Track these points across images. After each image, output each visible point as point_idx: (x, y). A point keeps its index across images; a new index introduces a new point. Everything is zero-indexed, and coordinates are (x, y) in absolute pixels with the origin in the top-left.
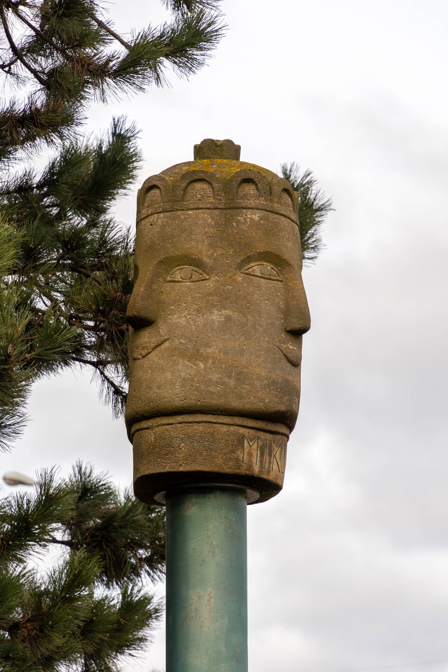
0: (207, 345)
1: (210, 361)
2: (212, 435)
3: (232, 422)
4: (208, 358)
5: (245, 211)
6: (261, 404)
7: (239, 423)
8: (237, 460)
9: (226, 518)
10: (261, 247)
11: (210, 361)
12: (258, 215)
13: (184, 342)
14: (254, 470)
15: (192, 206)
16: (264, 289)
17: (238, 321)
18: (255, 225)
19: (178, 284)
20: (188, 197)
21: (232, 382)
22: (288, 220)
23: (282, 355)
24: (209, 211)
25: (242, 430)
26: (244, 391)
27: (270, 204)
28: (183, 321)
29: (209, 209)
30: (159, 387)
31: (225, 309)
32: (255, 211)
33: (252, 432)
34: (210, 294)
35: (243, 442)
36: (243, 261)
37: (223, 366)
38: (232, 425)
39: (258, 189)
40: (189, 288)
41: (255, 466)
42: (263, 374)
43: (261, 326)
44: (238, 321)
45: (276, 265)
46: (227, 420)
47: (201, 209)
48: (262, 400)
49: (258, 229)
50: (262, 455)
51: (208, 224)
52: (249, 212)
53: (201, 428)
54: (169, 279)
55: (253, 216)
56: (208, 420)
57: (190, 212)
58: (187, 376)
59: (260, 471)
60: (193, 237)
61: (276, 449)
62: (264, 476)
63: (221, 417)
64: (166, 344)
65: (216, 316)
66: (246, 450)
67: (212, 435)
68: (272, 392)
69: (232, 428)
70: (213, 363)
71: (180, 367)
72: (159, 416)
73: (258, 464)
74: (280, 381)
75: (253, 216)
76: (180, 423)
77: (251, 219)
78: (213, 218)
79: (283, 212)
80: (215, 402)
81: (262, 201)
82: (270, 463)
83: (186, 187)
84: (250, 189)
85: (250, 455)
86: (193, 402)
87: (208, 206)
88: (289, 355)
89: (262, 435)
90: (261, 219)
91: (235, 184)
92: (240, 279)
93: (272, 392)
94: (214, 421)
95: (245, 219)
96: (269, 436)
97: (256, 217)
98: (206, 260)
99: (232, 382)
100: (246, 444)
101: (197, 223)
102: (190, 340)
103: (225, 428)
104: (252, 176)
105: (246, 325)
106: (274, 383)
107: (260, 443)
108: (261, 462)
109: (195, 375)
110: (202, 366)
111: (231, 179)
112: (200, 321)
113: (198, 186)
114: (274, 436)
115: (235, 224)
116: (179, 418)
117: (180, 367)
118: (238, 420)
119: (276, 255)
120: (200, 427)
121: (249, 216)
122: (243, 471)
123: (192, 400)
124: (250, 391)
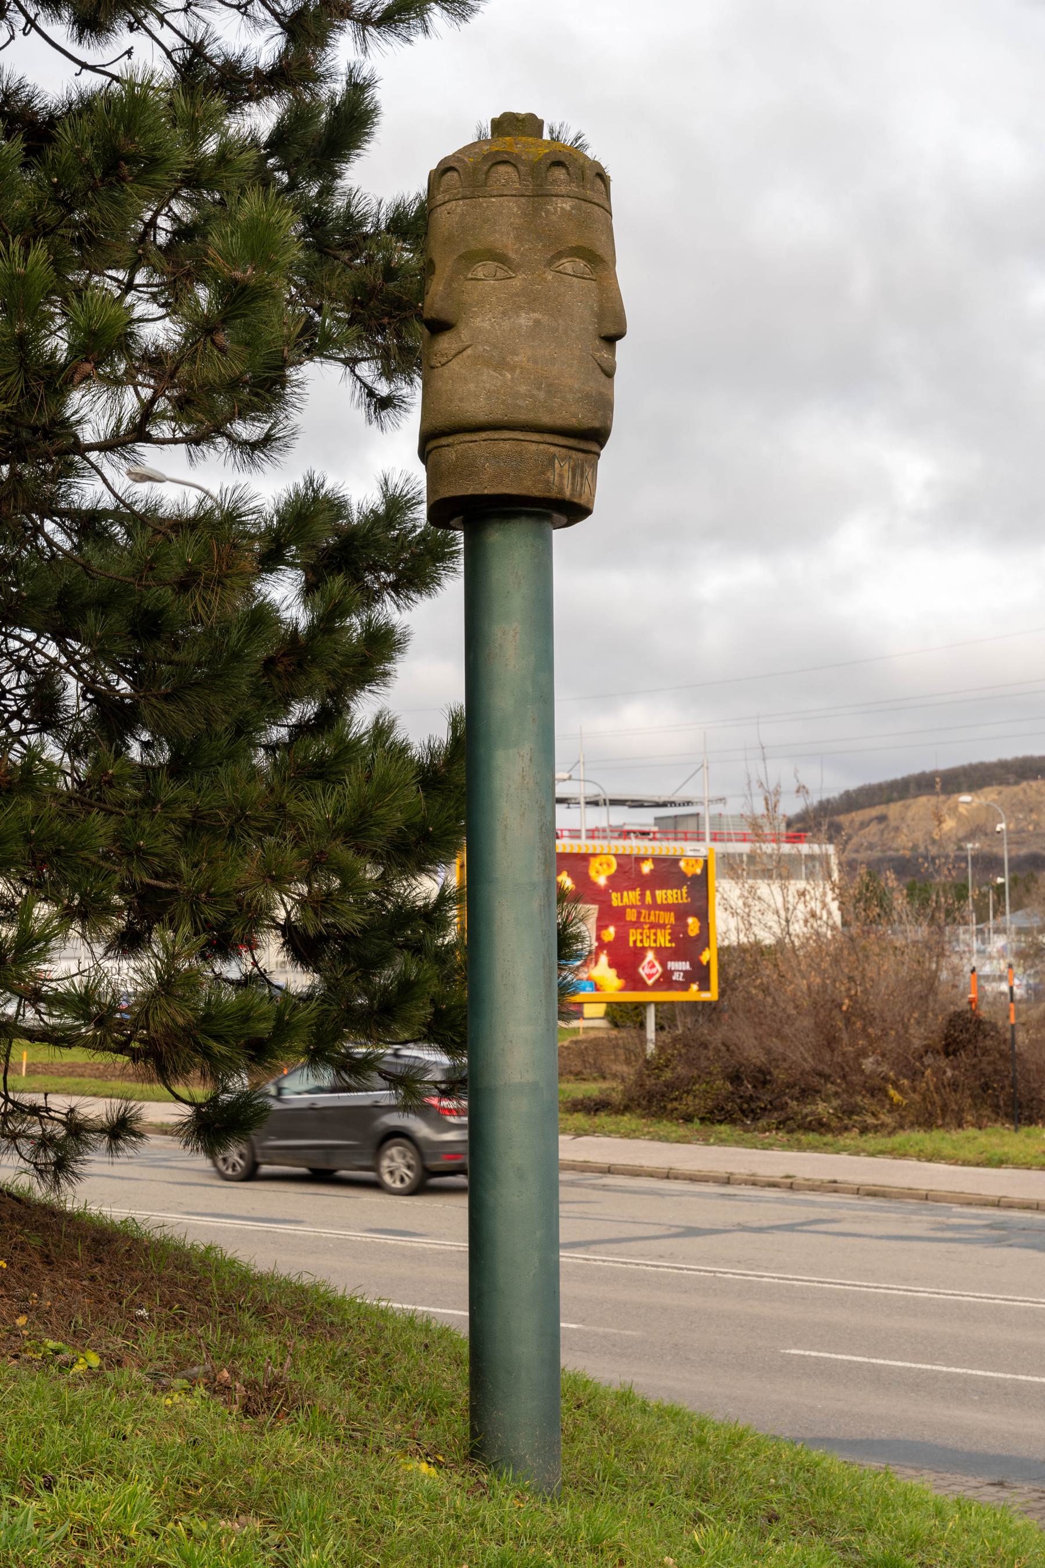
2: (520, 453)
5: (554, 199)
8: (548, 482)
10: (573, 241)
11: (518, 371)
15: (495, 193)
21: (542, 395)
25: (553, 449)
28: (486, 325)
30: (461, 400)
31: (534, 311)
33: (564, 450)
34: (517, 295)
36: (553, 257)
39: (569, 174)
42: (576, 386)
45: (589, 261)
46: (536, 437)
48: (575, 415)
52: (559, 200)
53: (508, 446)
54: (470, 276)
57: (493, 200)
59: (572, 495)
60: (497, 228)
64: (469, 351)
65: (524, 320)
66: (557, 471)
67: (520, 453)
69: (542, 447)
73: (570, 486)
77: (562, 208)
78: (519, 207)
80: (523, 417)
81: (574, 188)
83: (489, 170)
84: (560, 174)
85: (561, 476)
86: (500, 417)
87: (514, 192)
88: (604, 365)
89: (573, 454)
95: (555, 208)
96: (581, 455)
98: (512, 255)
99: (542, 395)
102: (495, 347)
103: (534, 447)
104: (563, 159)
105: (557, 330)
106: (588, 396)
108: (573, 484)
109: (502, 386)
110: (509, 376)
111: (539, 162)
112: (506, 324)
116: (484, 435)
117: (485, 378)
120: (507, 446)
122: (554, 494)
123: (499, 414)
124: (562, 405)
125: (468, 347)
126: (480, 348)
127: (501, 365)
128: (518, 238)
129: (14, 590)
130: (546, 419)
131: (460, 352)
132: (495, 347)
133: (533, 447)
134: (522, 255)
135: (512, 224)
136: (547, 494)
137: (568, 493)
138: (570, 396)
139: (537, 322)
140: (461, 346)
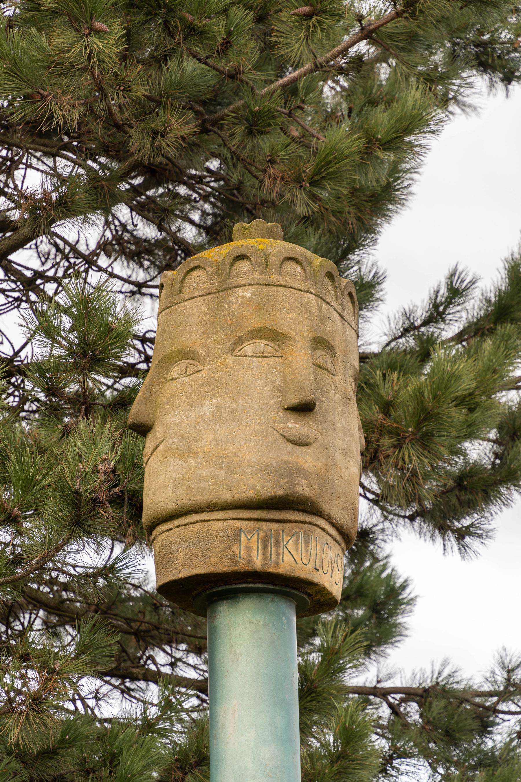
0: (198, 440)
1: (201, 456)
2: (207, 533)
3: (226, 517)
4: (199, 452)
5: (236, 290)
6: (252, 492)
7: (234, 517)
8: (234, 556)
9: (251, 622)
10: (253, 324)
11: (201, 456)
12: (250, 291)
13: (176, 440)
14: (254, 564)
15: (187, 297)
16: (255, 368)
17: (229, 407)
18: (249, 302)
19: (175, 382)
20: (185, 289)
21: (222, 474)
22: (291, 290)
23: (278, 435)
24: (202, 298)
25: (238, 524)
26: (235, 481)
27: (264, 276)
28: (176, 419)
29: (203, 295)
30: (154, 493)
31: (216, 397)
32: (246, 288)
33: (251, 523)
34: (202, 385)
35: (240, 536)
36: (234, 343)
37: (214, 459)
38: (227, 519)
39: (252, 264)
40: (184, 384)
41: (255, 559)
42: (254, 459)
43: (252, 408)
44: (229, 407)
45: (273, 340)
46: (221, 515)
47: (196, 297)
48: (253, 488)
49: (249, 305)
50: (265, 547)
51: (201, 312)
52: (241, 290)
53: (196, 528)
54: (169, 378)
55: (245, 293)
56: (202, 519)
57: (186, 303)
58: (179, 476)
59: (264, 565)
60: (188, 328)
61: (286, 539)
62: (271, 570)
63: (214, 513)
64: (162, 447)
65: (208, 407)
66: (243, 544)
67: (207, 533)
68: (265, 477)
69: (227, 523)
70: (204, 457)
71: (172, 468)
72: (159, 524)
73: (260, 557)
74: (274, 464)
75: (245, 293)
76: (177, 527)
77: (243, 297)
78: (206, 305)
79: (282, 283)
80: (204, 498)
81: (257, 276)
82: (278, 555)
83: (184, 278)
84: (243, 266)
85: (249, 548)
86: (185, 501)
87: (202, 293)
88: (288, 435)
89: (264, 525)
90: (253, 294)
91: (227, 264)
92: (231, 362)
93: (265, 477)
94: (208, 518)
95: (237, 299)
96: (274, 526)
97: (248, 294)
98: (199, 350)
99: (222, 474)
100: (243, 537)
101: (191, 313)
102: (182, 437)
103: (220, 525)
104: (244, 252)
105: (237, 410)
106: (267, 467)
107: (262, 534)
108: (264, 554)
109: (186, 473)
110: (193, 462)
111: (224, 260)
112: (193, 415)
113: (195, 274)
114: (282, 525)
115: (226, 306)
116: (176, 522)
117: (172, 468)
118: (232, 514)
119: (271, 330)
120: (195, 528)
121: (240, 295)
122: (242, 567)
123: (185, 500)
124: (241, 480)
125: (160, 443)
126: (170, 441)
127: (185, 453)
128: (205, 334)
129: (432, 745)
130: (225, 496)
131: (155, 449)
132: (182, 437)
133: (219, 525)
134: (208, 347)
135: (200, 321)
136: (234, 568)
137: (258, 564)
138: (248, 470)
139: (219, 407)
140: (158, 441)
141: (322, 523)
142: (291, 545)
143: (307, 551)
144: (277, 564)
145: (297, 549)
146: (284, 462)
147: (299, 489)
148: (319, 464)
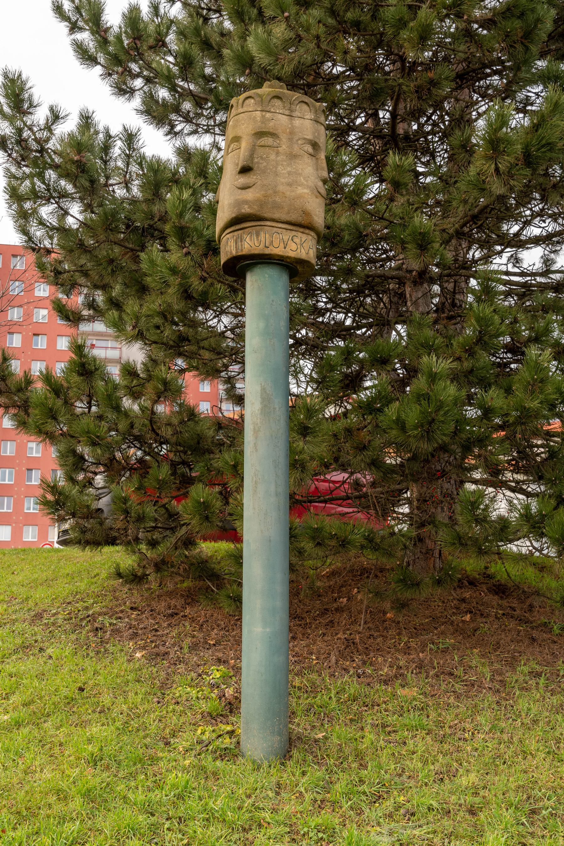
33: (231, 234)
59: (237, 252)
61: (245, 236)
88: (238, 186)
89: (236, 233)
96: (240, 232)
141: (268, 223)
142: (248, 240)
143: (258, 240)
144: (242, 250)
145: (251, 240)
146: (236, 200)
147: (243, 211)
148: (258, 195)
